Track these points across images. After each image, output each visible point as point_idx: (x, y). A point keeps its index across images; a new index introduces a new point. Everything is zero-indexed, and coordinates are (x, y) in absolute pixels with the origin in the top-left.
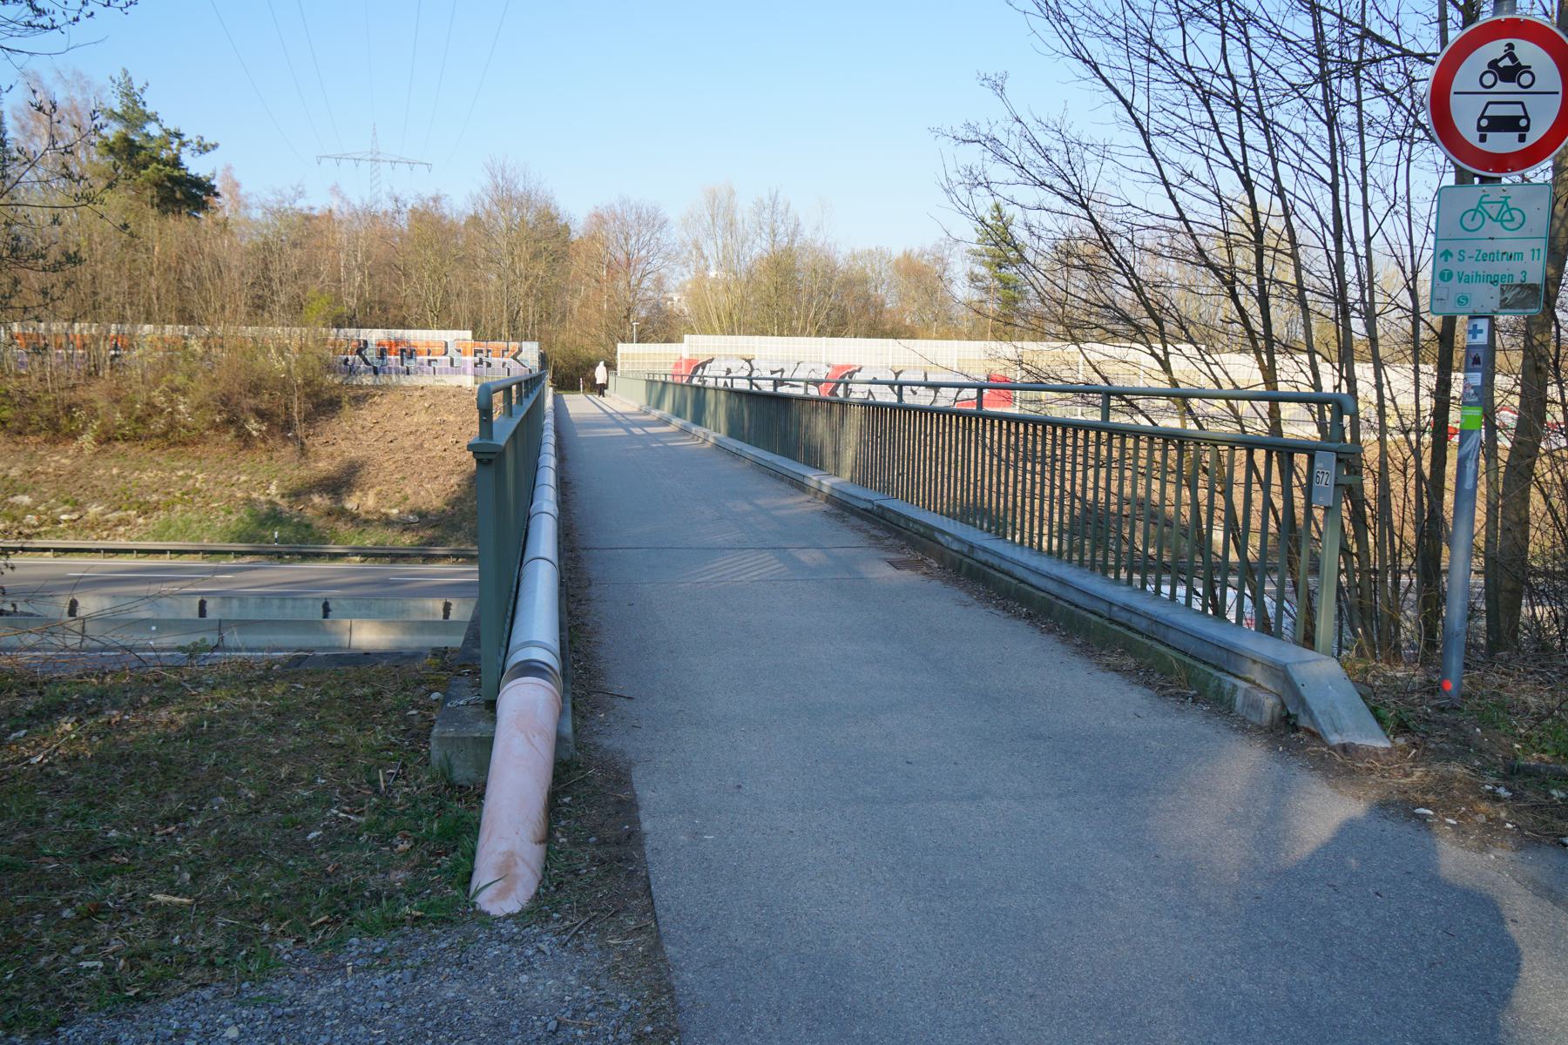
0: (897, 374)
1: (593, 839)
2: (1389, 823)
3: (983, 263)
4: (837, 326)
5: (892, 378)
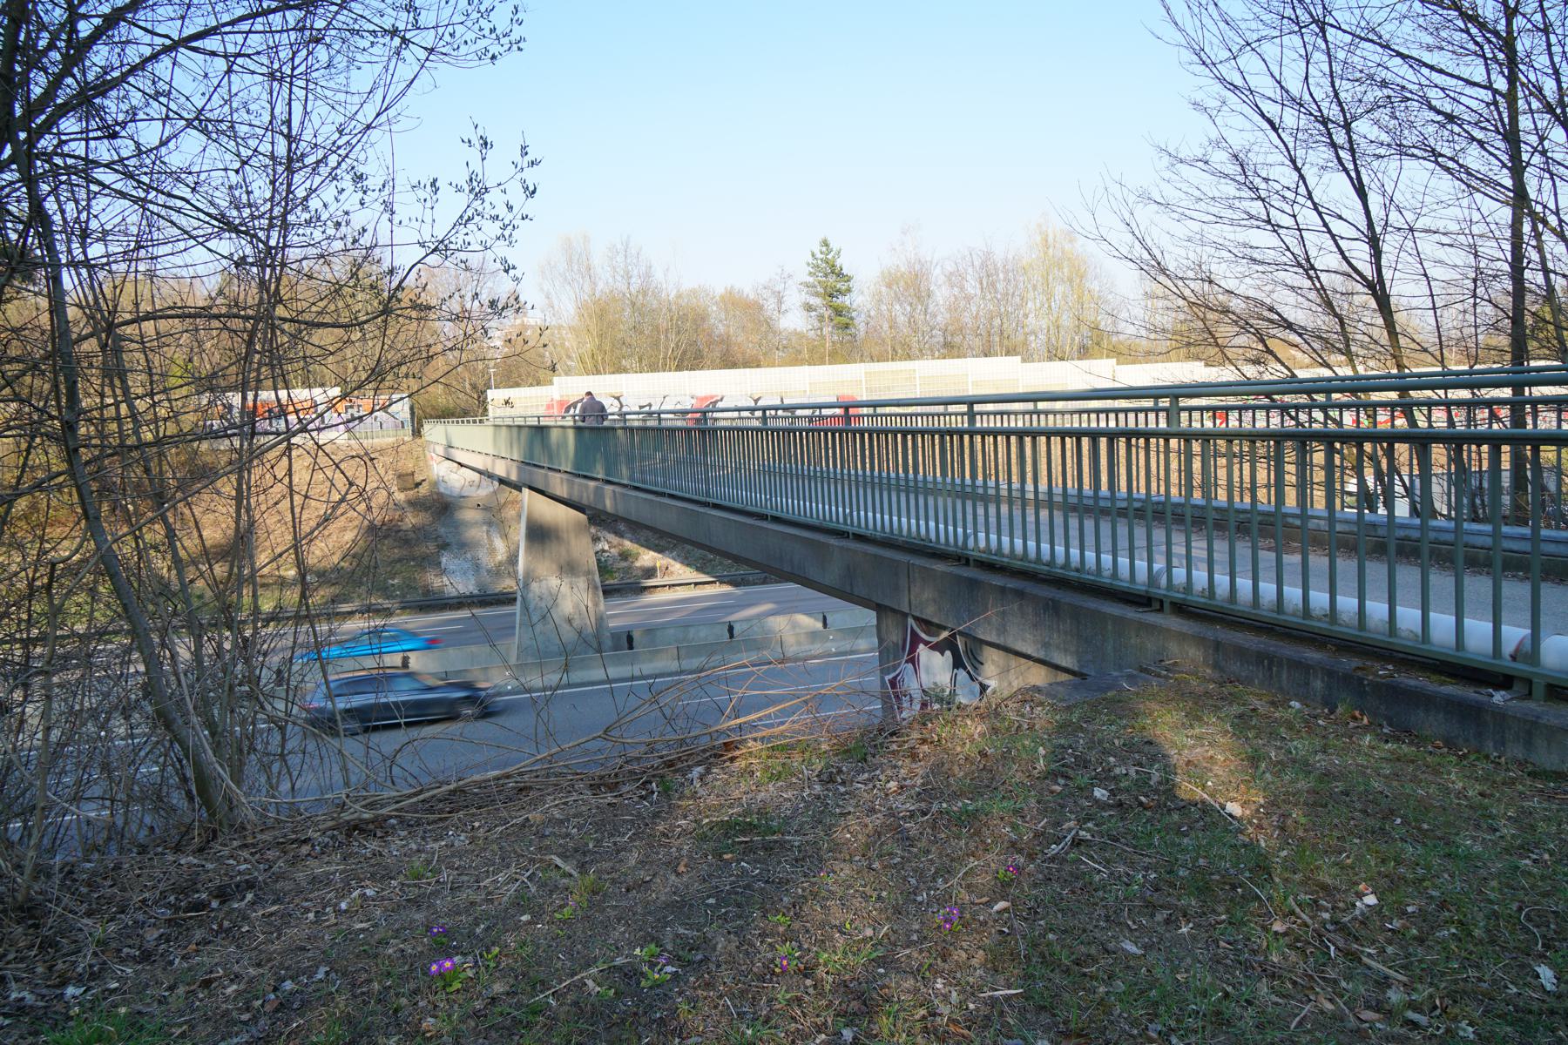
0: (756, 401)
1: (259, 625)
2: (317, 542)
3: (817, 294)
4: (689, 359)
5: (752, 404)
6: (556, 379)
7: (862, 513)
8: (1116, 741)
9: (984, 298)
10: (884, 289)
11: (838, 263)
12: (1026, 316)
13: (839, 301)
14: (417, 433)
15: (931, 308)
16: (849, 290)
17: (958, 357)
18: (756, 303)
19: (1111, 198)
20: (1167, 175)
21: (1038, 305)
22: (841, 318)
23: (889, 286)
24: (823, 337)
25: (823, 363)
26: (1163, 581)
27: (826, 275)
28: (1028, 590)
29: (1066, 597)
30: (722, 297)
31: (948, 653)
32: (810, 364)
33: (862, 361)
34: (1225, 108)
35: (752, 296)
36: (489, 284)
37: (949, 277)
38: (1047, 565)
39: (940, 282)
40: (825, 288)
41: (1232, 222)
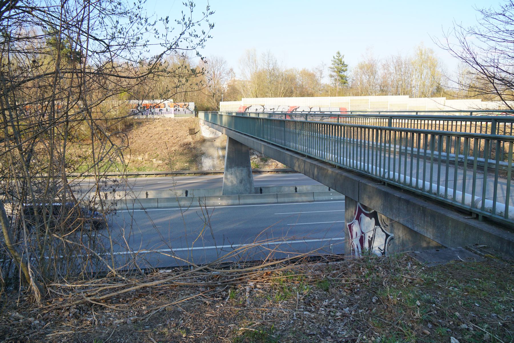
0: (311, 109)
3: (334, 71)
4: (289, 93)
6: (243, 99)
8: (460, 302)
9: (396, 74)
12: (412, 81)
13: (343, 73)
14: (196, 115)
15: (376, 77)
16: (346, 70)
17: (385, 95)
18: (313, 74)
20: (483, 21)
21: (417, 77)
22: (343, 80)
23: (361, 68)
25: (335, 96)
26: (480, 205)
27: (338, 65)
30: (301, 72)
31: (373, 219)
32: (331, 96)
33: (349, 96)
37: (384, 66)
38: (421, 190)
39: (380, 68)
40: (338, 69)
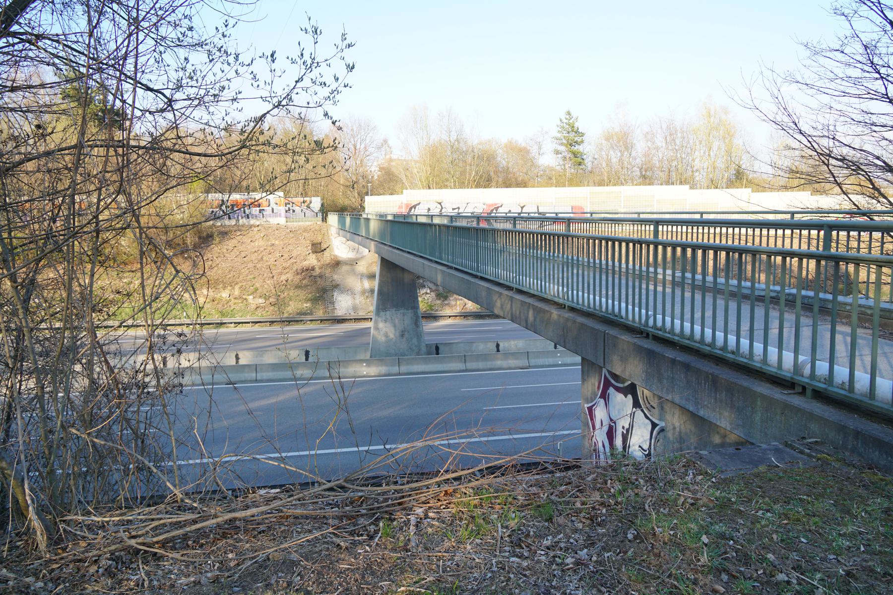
0: (522, 208)
3: (562, 144)
4: (485, 182)
7: (575, 292)
8: (775, 536)
10: (604, 141)
11: (576, 125)
12: (693, 160)
13: (577, 148)
15: (633, 154)
16: (582, 142)
17: (649, 184)
18: (525, 148)
19: (765, 80)
21: (702, 154)
22: (577, 159)
23: (607, 139)
24: (565, 170)
25: (564, 186)
26: (807, 371)
28: (693, 364)
29: (725, 374)
31: (630, 397)
34: (856, 15)
35: (523, 145)
36: (371, 134)
41: (859, 97)
